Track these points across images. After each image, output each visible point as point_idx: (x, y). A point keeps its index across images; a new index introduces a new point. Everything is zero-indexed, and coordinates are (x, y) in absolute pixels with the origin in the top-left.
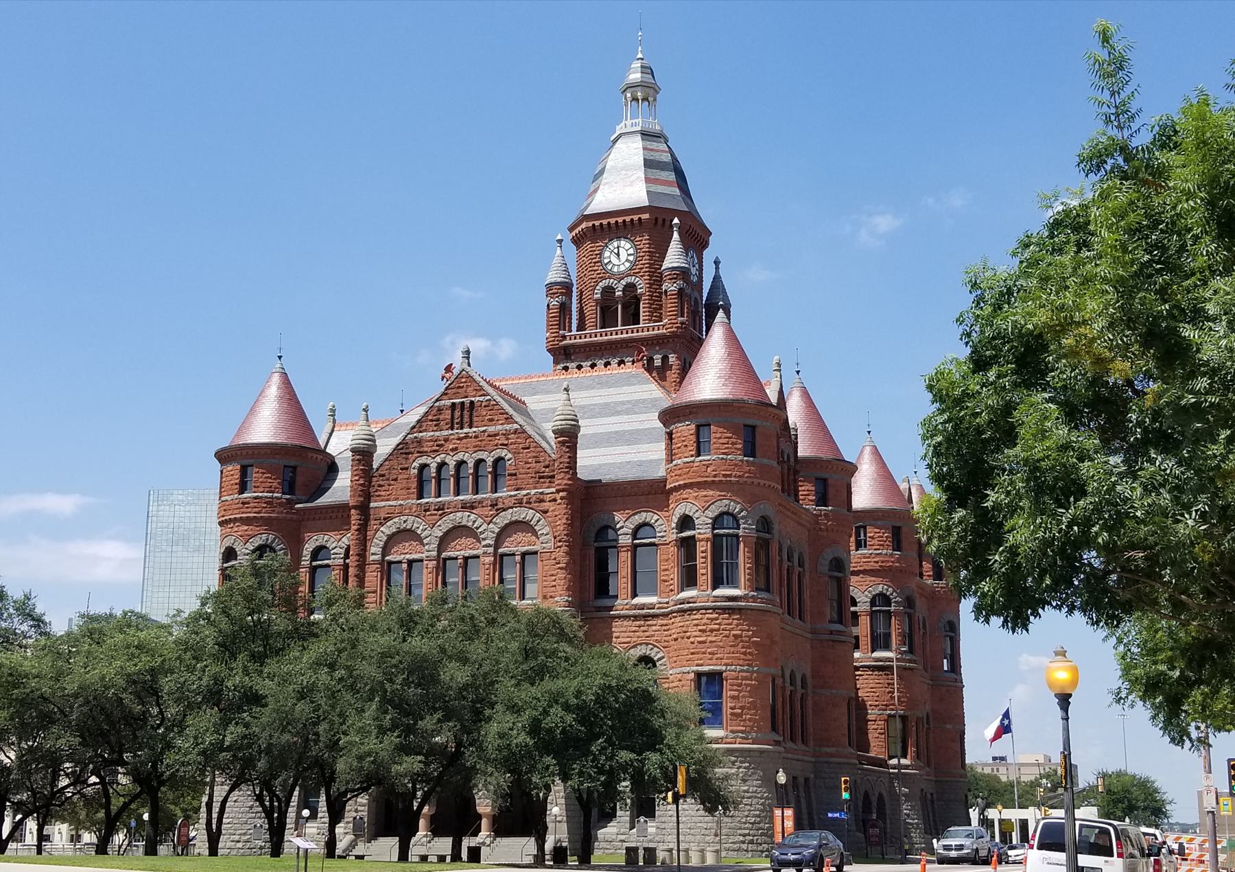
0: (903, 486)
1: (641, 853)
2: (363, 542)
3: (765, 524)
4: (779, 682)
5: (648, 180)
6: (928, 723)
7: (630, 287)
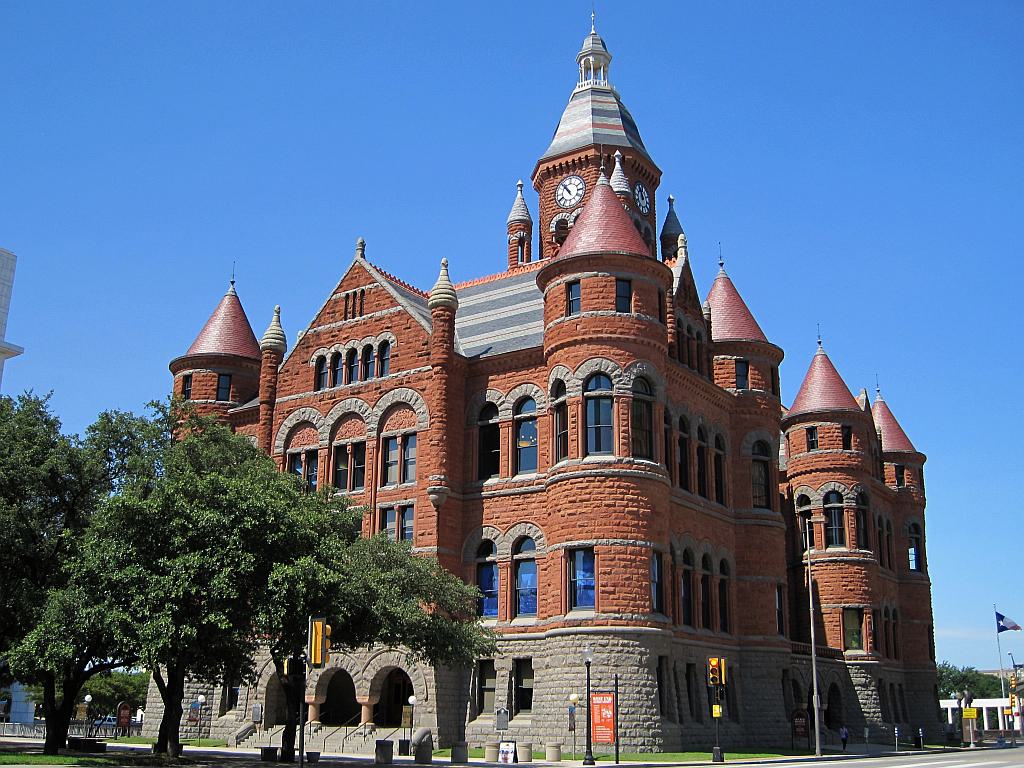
4: (667, 558)
5: (594, 125)
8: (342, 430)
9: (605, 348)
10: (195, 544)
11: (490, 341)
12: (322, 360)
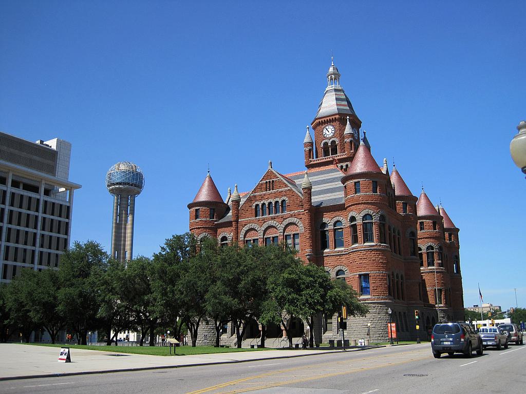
0: (437, 208)
1: (335, 342)
2: (237, 233)
3: (382, 218)
5: (337, 105)
6: (450, 291)
7: (333, 142)
8: (268, 232)
9: (370, 206)
10: (307, 287)
11: (322, 199)
12: (257, 205)
